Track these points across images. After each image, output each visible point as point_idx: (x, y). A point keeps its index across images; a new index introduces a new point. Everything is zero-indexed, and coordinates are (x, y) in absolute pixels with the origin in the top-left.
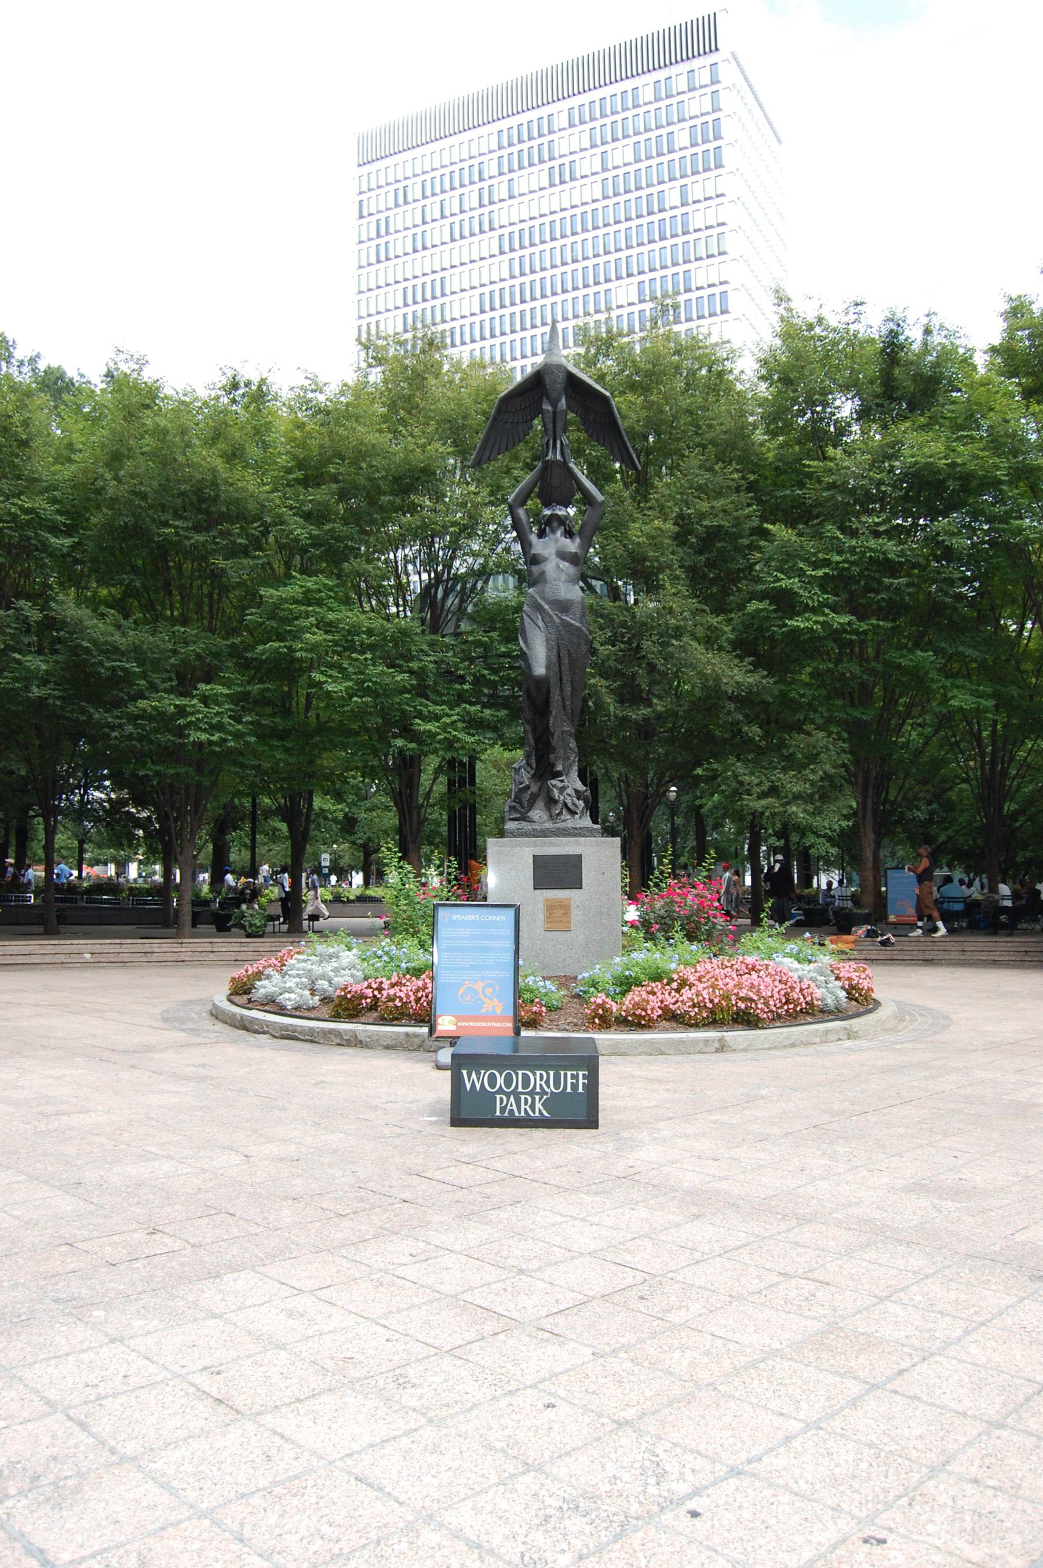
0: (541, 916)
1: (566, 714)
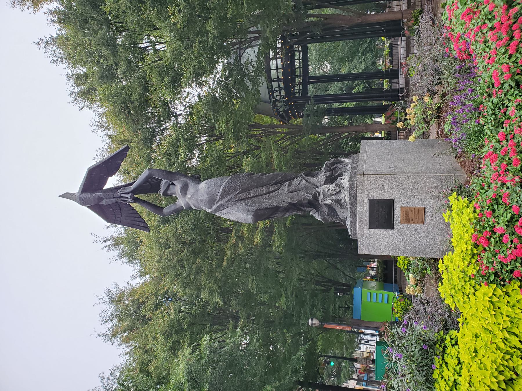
0: (413, 226)
1: (280, 188)
